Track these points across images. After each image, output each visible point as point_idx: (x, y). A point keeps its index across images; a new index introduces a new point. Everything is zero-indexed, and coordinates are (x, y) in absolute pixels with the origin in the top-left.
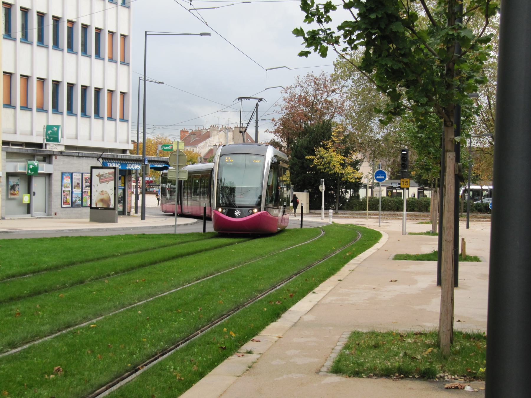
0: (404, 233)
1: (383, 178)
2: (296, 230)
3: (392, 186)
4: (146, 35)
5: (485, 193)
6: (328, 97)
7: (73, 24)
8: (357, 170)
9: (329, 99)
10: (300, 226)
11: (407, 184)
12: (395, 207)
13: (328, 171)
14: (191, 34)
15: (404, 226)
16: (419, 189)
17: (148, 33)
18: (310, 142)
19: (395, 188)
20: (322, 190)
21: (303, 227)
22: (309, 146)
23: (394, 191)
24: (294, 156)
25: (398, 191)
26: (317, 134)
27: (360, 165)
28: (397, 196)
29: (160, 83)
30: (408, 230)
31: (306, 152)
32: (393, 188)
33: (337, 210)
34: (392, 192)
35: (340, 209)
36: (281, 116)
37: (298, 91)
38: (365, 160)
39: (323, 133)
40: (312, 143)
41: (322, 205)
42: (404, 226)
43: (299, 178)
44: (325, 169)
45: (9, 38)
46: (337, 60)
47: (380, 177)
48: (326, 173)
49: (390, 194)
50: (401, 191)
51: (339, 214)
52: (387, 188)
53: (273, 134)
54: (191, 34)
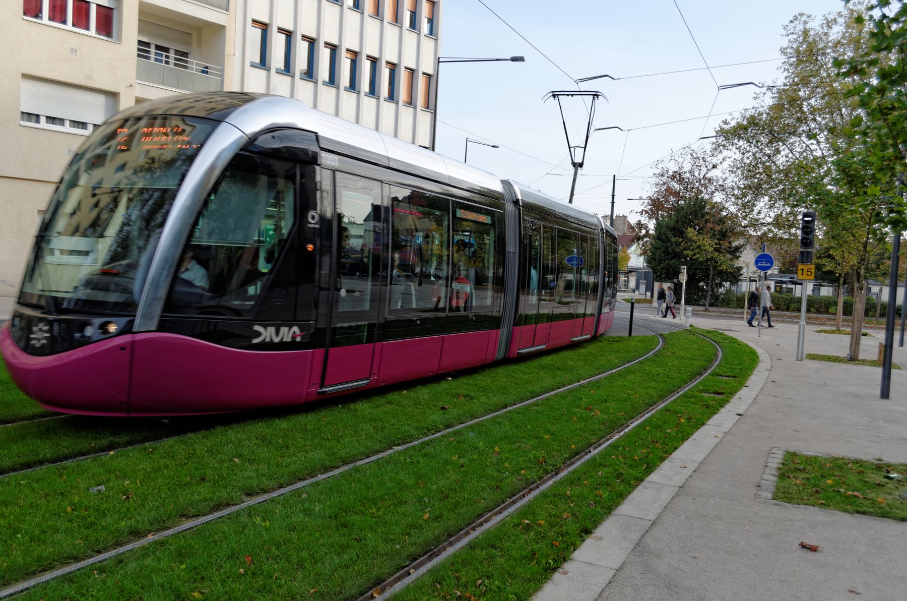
0: (799, 358)
1: (769, 265)
2: (620, 340)
3: (782, 281)
4: (439, 62)
5: (383, 287)
6: (707, 173)
7: (356, 56)
8: (738, 258)
9: (708, 176)
10: (628, 333)
11: (809, 273)
12: (743, 120)
13: (699, 258)
14: (498, 60)
15: (801, 340)
16: (815, 285)
17: (441, 60)
18: (677, 222)
19: (785, 283)
20: (683, 280)
21: (633, 334)
22: (677, 226)
23: (784, 286)
24: (657, 239)
25: (789, 286)
26: (687, 213)
27: (741, 252)
28: (788, 292)
29: (494, 146)
30: (810, 349)
31: (672, 234)
32: (782, 282)
33: (707, 306)
34: (781, 286)
35: (711, 305)
36: (651, 194)
37: (673, 168)
38: (748, 247)
39: (695, 211)
40: (680, 223)
41: (681, 300)
42: (801, 340)
43: (662, 265)
44: (695, 254)
45: (264, 68)
46: (720, 127)
47: (764, 264)
48: (695, 260)
49: (778, 289)
50: (793, 286)
51: (709, 312)
52: (776, 283)
53: (638, 214)
54: (498, 60)
